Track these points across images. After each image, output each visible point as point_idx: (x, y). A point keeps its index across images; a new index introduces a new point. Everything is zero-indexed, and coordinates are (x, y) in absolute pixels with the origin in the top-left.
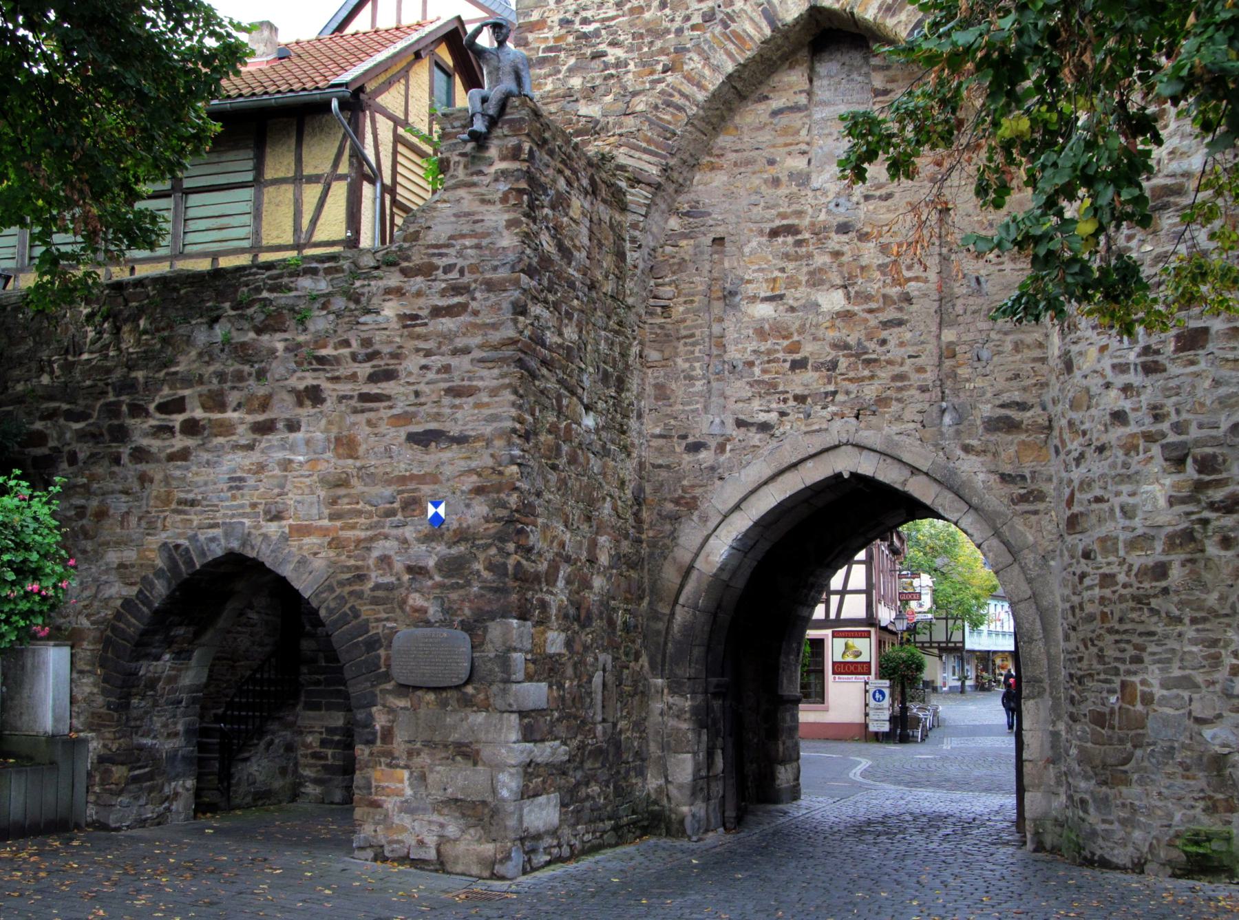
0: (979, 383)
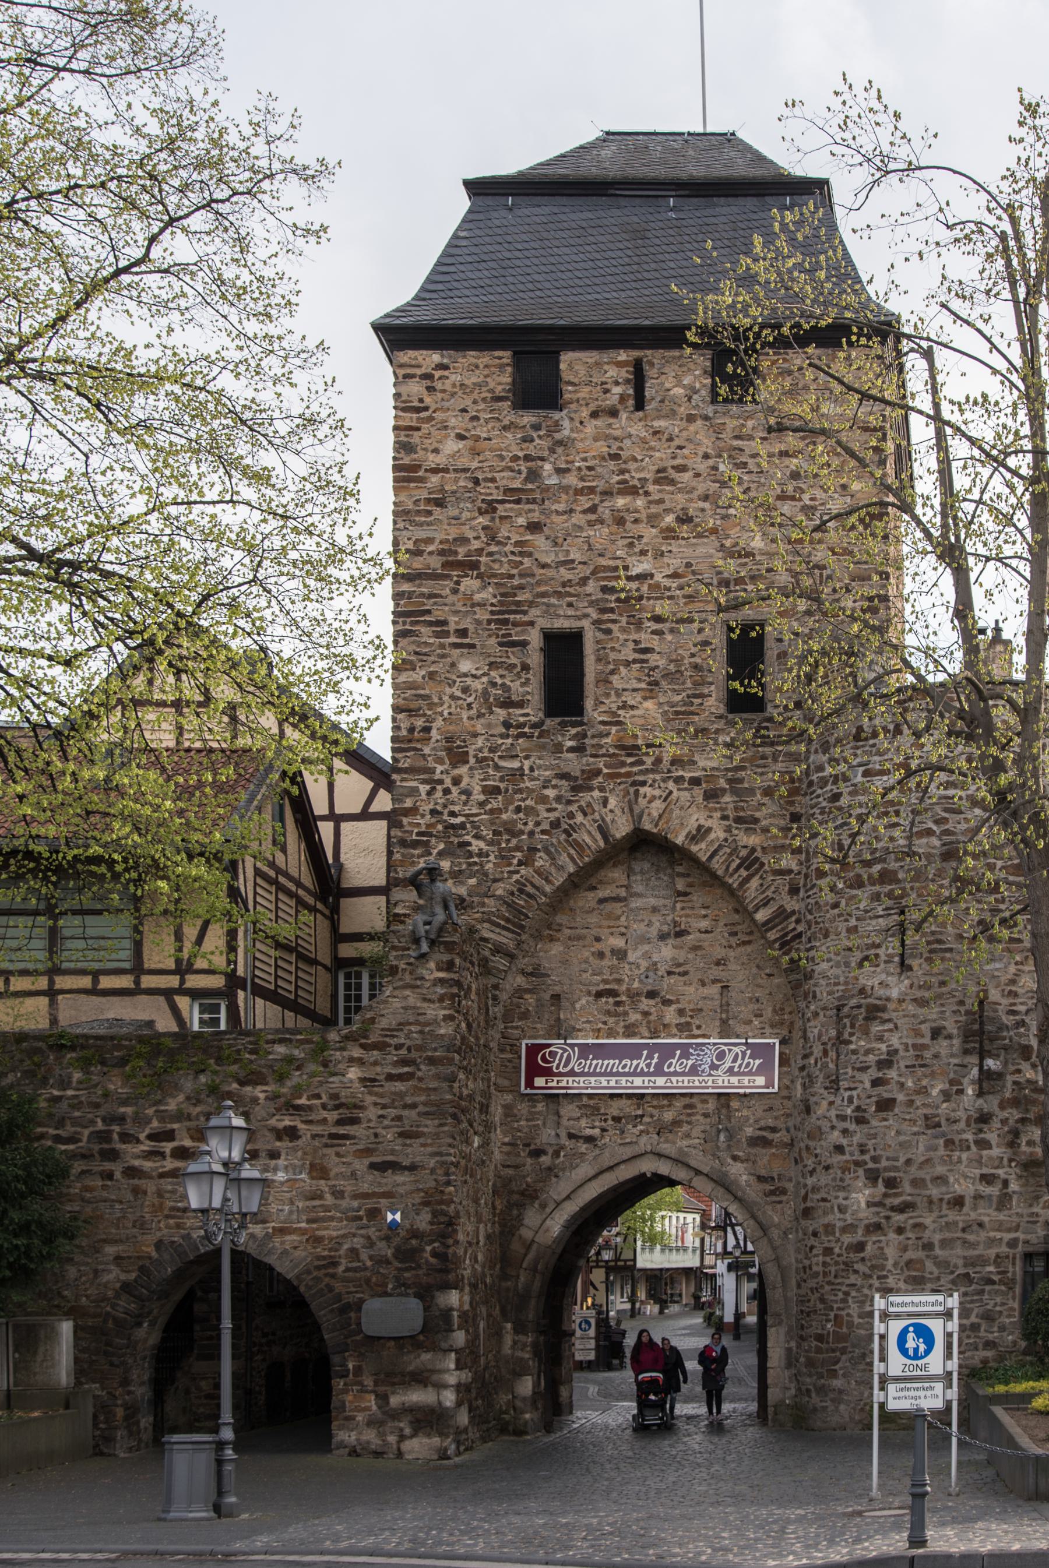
0: (745, 1112)
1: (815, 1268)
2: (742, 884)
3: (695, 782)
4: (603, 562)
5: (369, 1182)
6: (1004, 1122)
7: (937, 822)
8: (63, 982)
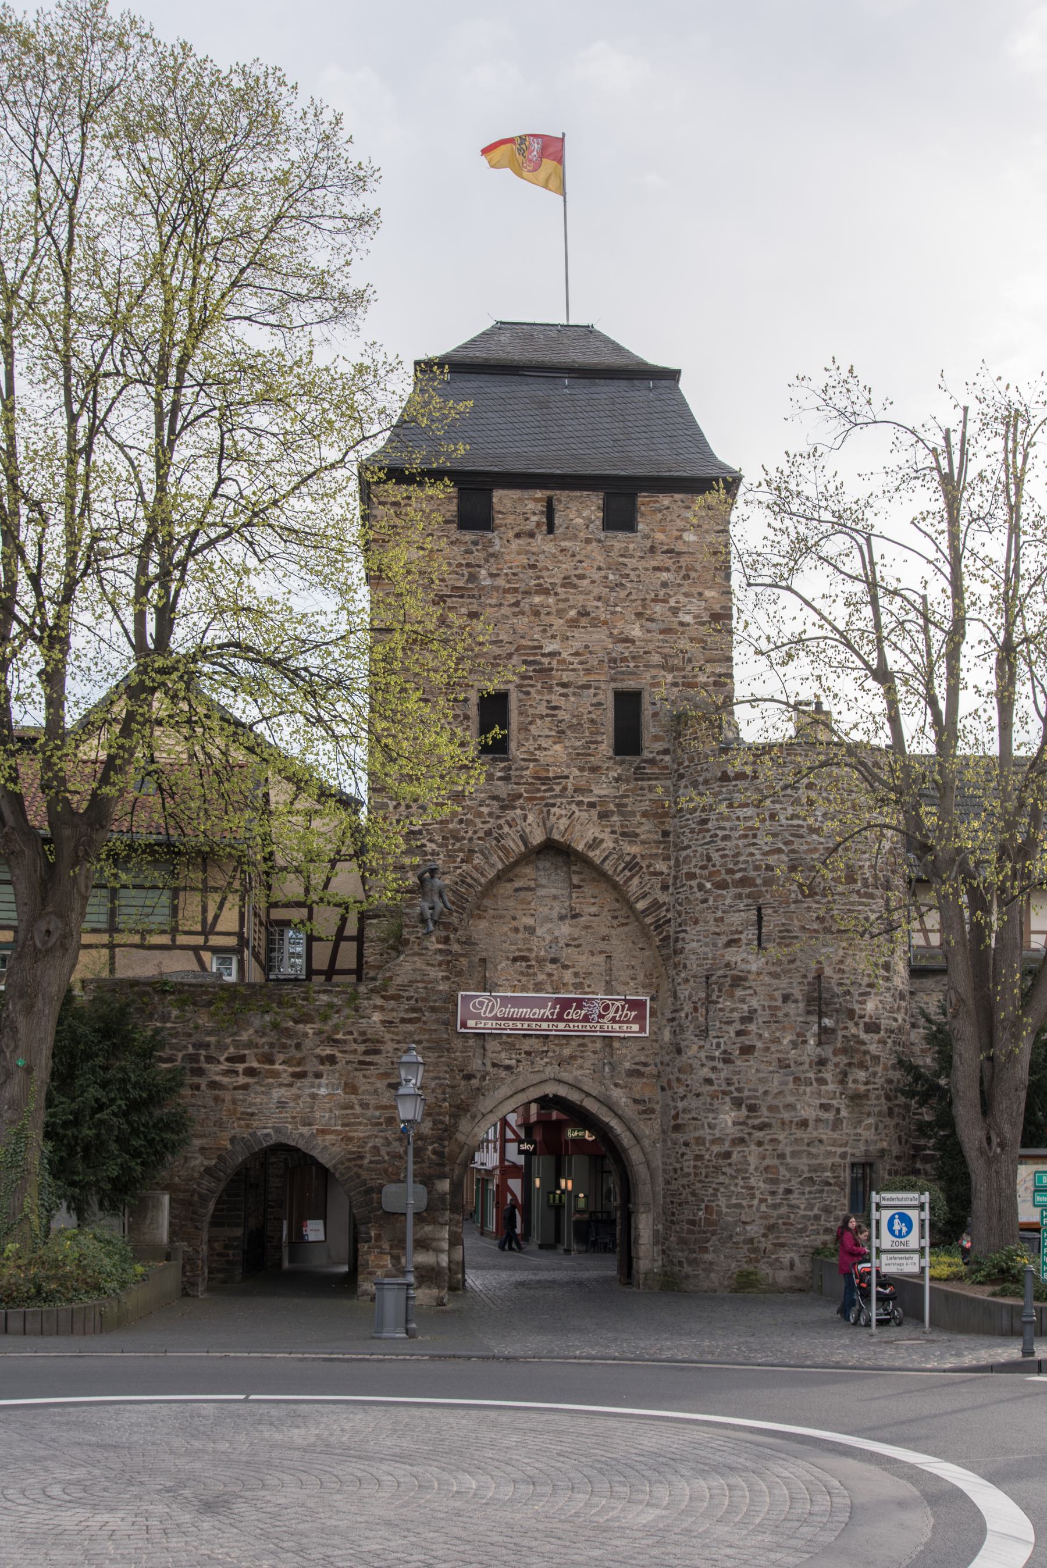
0: (624, 1051)
1: (686, 1170)
2: (626, 882)
3: (592, 805)
4: (524, 642)
6: (836, 1065)
7: (785, 843)
8: (118, 938)
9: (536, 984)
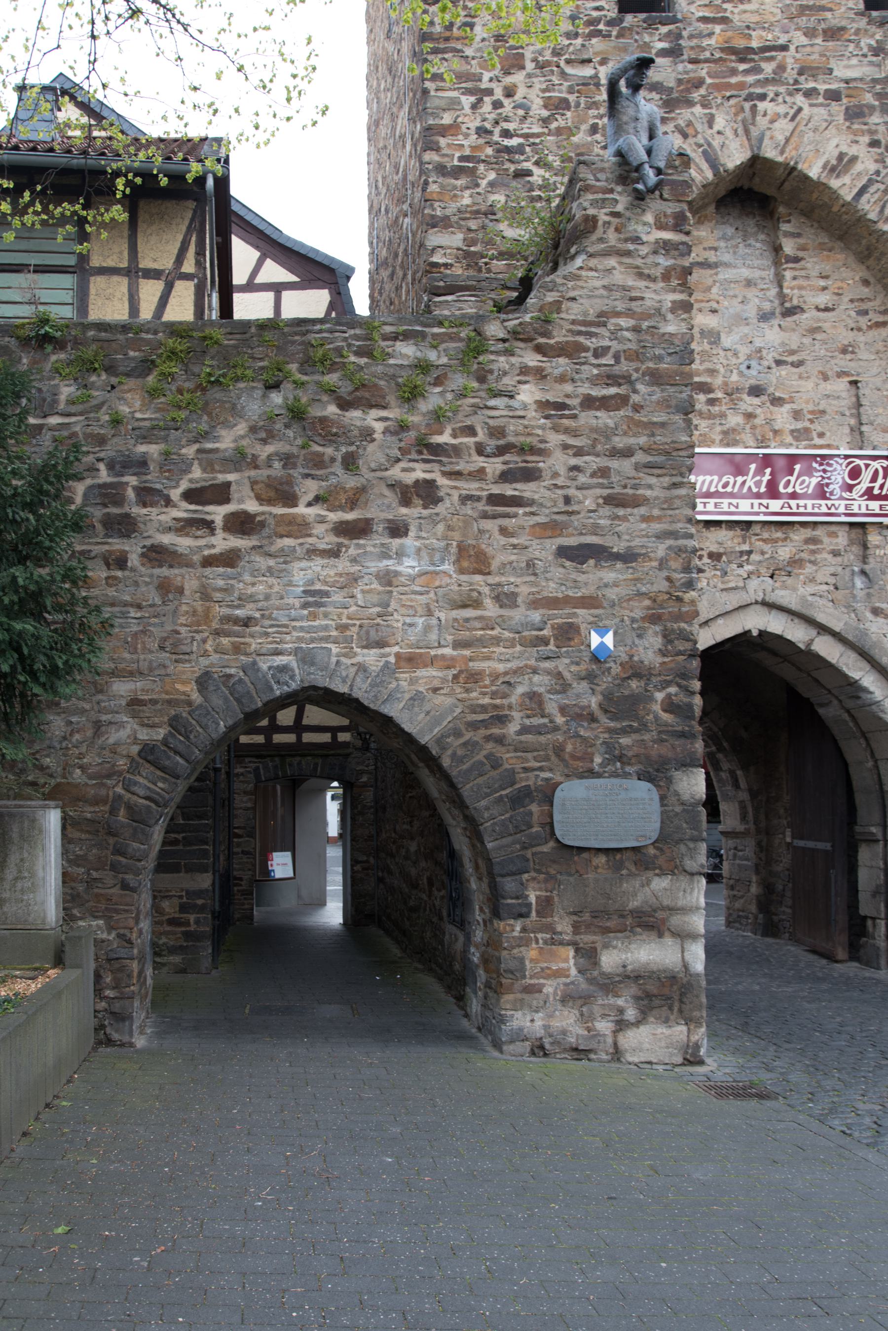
3: (833, 96)
5: (557, 579)
9: (725, 433)
